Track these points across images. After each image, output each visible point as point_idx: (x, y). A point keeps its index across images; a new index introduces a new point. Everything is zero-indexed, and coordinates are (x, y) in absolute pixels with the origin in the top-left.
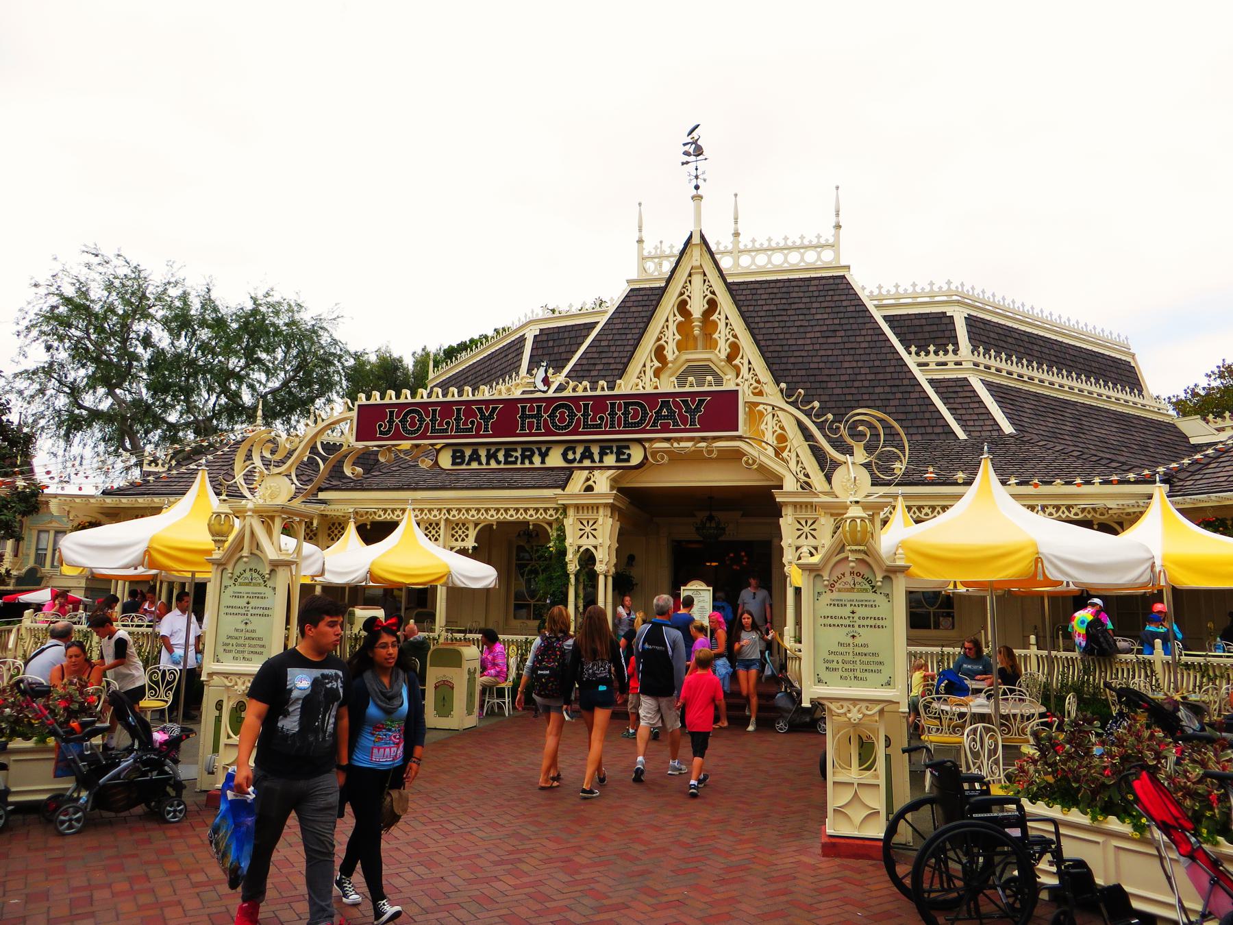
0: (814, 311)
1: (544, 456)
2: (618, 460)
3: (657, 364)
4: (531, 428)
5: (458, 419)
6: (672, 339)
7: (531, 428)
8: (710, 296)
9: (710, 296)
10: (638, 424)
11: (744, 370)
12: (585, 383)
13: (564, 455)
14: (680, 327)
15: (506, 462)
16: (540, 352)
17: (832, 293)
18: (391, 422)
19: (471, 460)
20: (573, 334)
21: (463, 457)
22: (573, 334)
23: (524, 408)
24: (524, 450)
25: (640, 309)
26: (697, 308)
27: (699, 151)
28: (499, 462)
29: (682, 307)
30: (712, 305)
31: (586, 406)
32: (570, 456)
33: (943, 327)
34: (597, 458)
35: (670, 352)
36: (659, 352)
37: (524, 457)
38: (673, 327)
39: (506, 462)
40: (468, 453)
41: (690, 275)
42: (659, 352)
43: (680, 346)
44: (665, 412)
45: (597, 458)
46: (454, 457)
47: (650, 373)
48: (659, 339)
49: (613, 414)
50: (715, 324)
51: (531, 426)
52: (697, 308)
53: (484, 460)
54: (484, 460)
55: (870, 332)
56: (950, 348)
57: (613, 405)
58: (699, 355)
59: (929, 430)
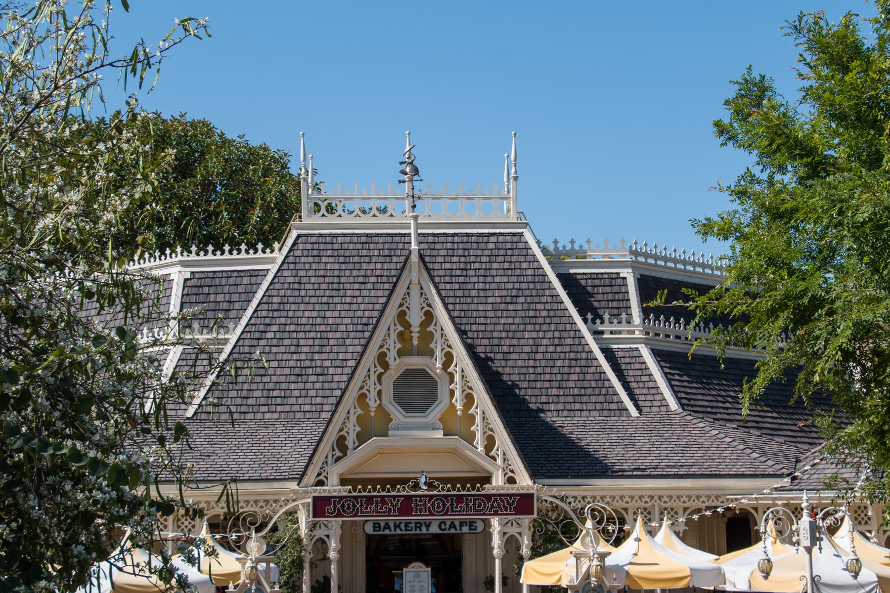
0: (494, 273)
1: (428, 526)
2: (470, 529)
3: (380, 370)
4: (421, 511)
5: (377, 506)
6: (394, 345)
7: (421, 511)
8: (427, 308)
9: (427, 308)
10: (480, 511)
11: (457, 378)
12: (449, 485)
13: (440, 526)
14: (401, 335)
15: (406, 530)
16: (193, 299)
17: (509, 247)
18: (335, 506)
19: (385, 528)
20: (231, 281)
21: (379, 527)
22: (231, 281)
23: (416, 500)
24: (416, 523)
25: (311, 260)
26: (415, 318)
27: (416, 171)
28: (401, 530)
29: (402, 316)
30: (429, 317)
31: (452, 500)
32: (443, 527)
33: (616, 289)
34: (458, 528)
35: (391, 356)
36: (382, 359)
37: (416, 527)
38: (394, 336)
39: (406, 530)
40: (383, 524)
41: (408, 288)
42: (382, 359)
43: (401, 353)
44: (495, 504)
45: (458, 528)
46: (374, 527)
47: (374, 377)
48: (381, 347)
49: (467, 505)
50: (431, 335)
51: (421, 510)
52: (415, 318)
53: (393, 529)
54: (393, 529)
55: (549, 299)
56: (624, 316)
57: (467, 500)
58: (415, 362)
59: (606, 406)
